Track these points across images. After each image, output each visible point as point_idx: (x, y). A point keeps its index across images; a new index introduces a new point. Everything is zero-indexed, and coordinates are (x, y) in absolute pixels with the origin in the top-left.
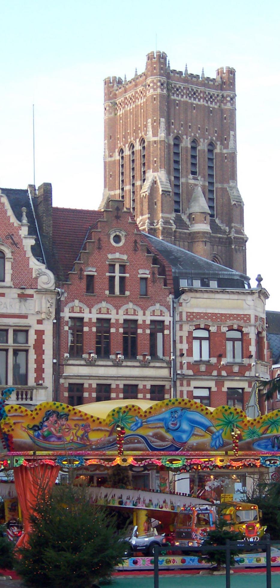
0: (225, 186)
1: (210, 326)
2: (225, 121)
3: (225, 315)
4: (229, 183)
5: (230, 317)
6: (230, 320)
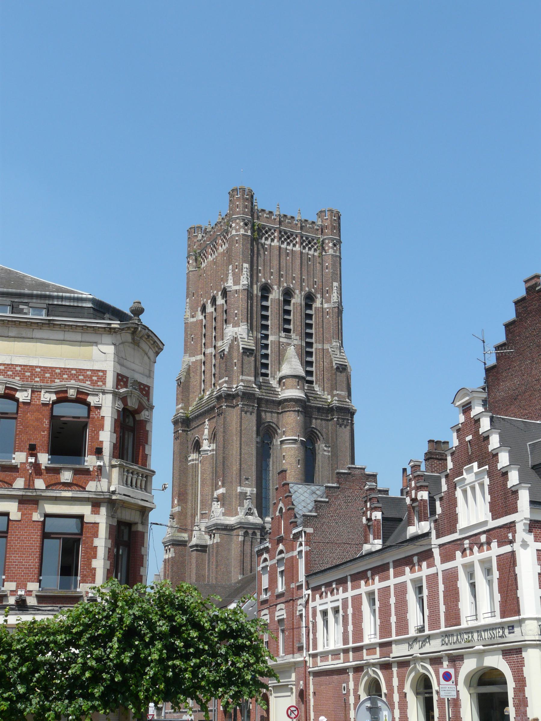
0: (326, 346)
1: (16, 390)
2: (327, 271)
3: (52, 369)
4: (331, 343)
5: (61, 375)
6: (62, 379)
